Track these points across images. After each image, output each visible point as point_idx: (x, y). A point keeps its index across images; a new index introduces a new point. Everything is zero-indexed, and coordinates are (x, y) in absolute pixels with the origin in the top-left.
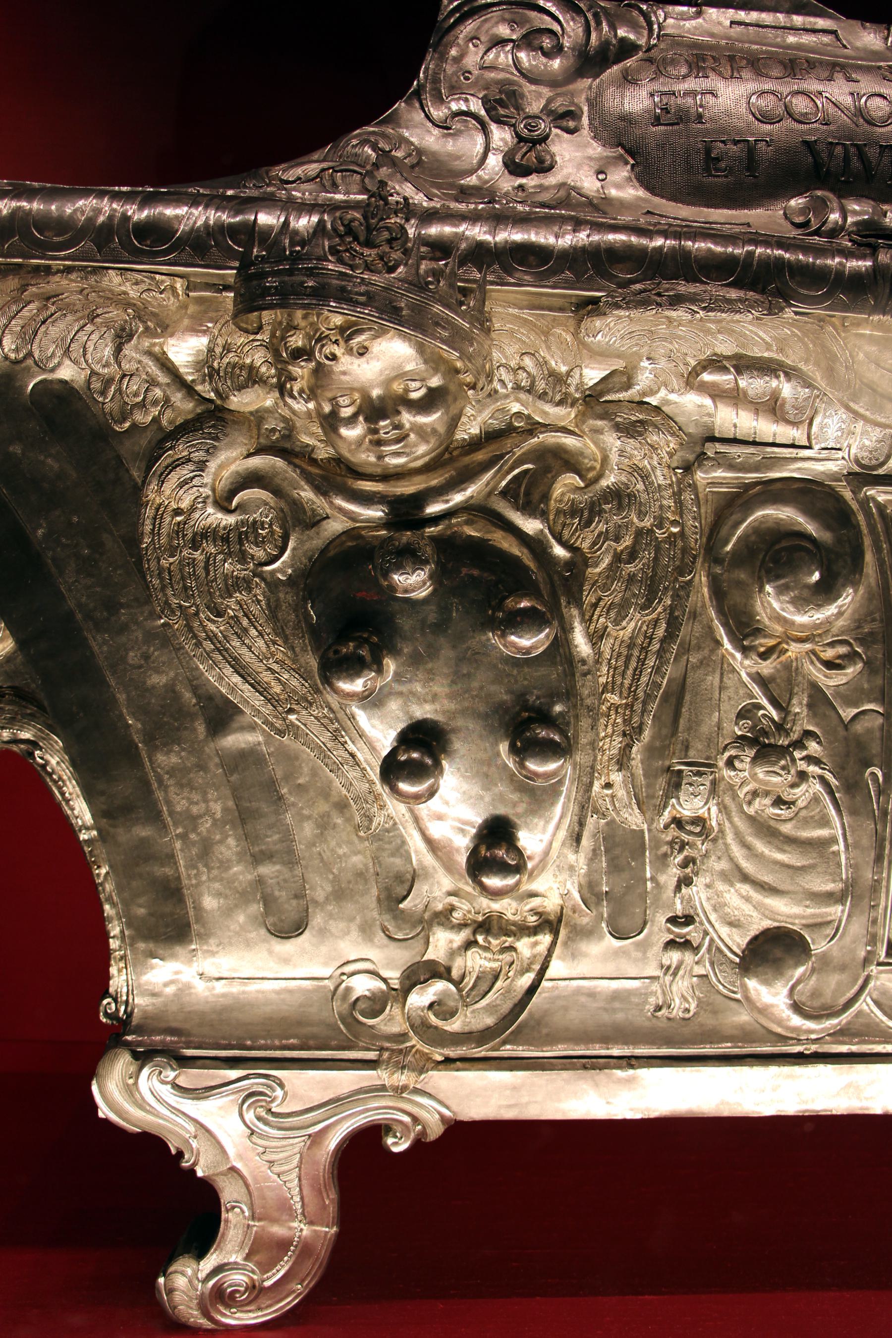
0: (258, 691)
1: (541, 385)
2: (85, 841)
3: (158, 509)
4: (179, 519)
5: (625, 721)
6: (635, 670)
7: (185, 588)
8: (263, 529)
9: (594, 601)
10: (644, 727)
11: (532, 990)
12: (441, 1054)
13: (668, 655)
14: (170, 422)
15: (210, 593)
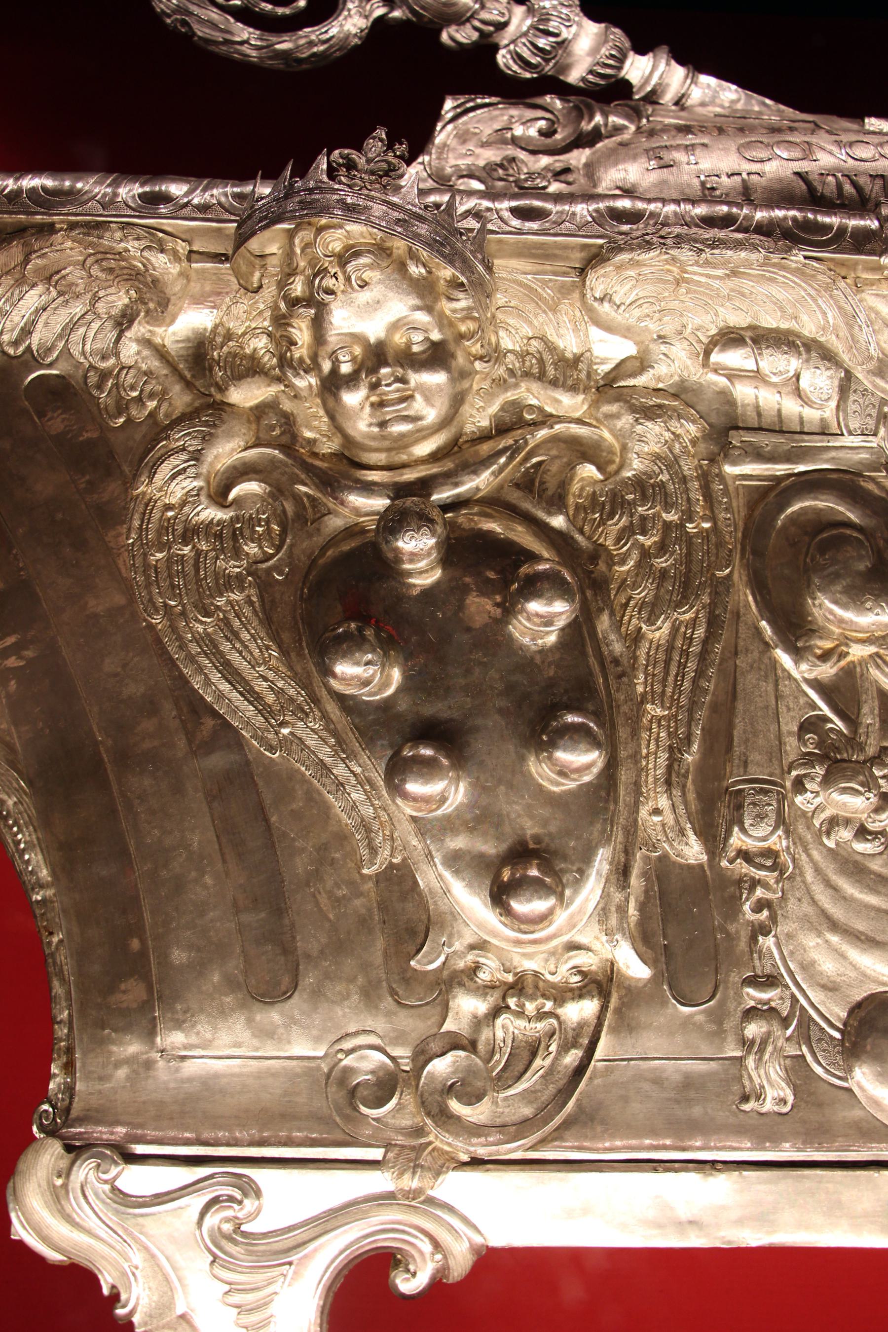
0: (246, 699)
1: (551, 372)
2: (37, 902)
3: (147, 505)
4: (170, 514)
5: (669, 734)
6: (677, 675)
7: (173, 586)
8: (260, 526)
9: (624, 601)
10: (693, 739)
11: (580, 1071)
12: (467, 1152)
13: (712, 656)
14: (167, 415)
15: (199, 593)
